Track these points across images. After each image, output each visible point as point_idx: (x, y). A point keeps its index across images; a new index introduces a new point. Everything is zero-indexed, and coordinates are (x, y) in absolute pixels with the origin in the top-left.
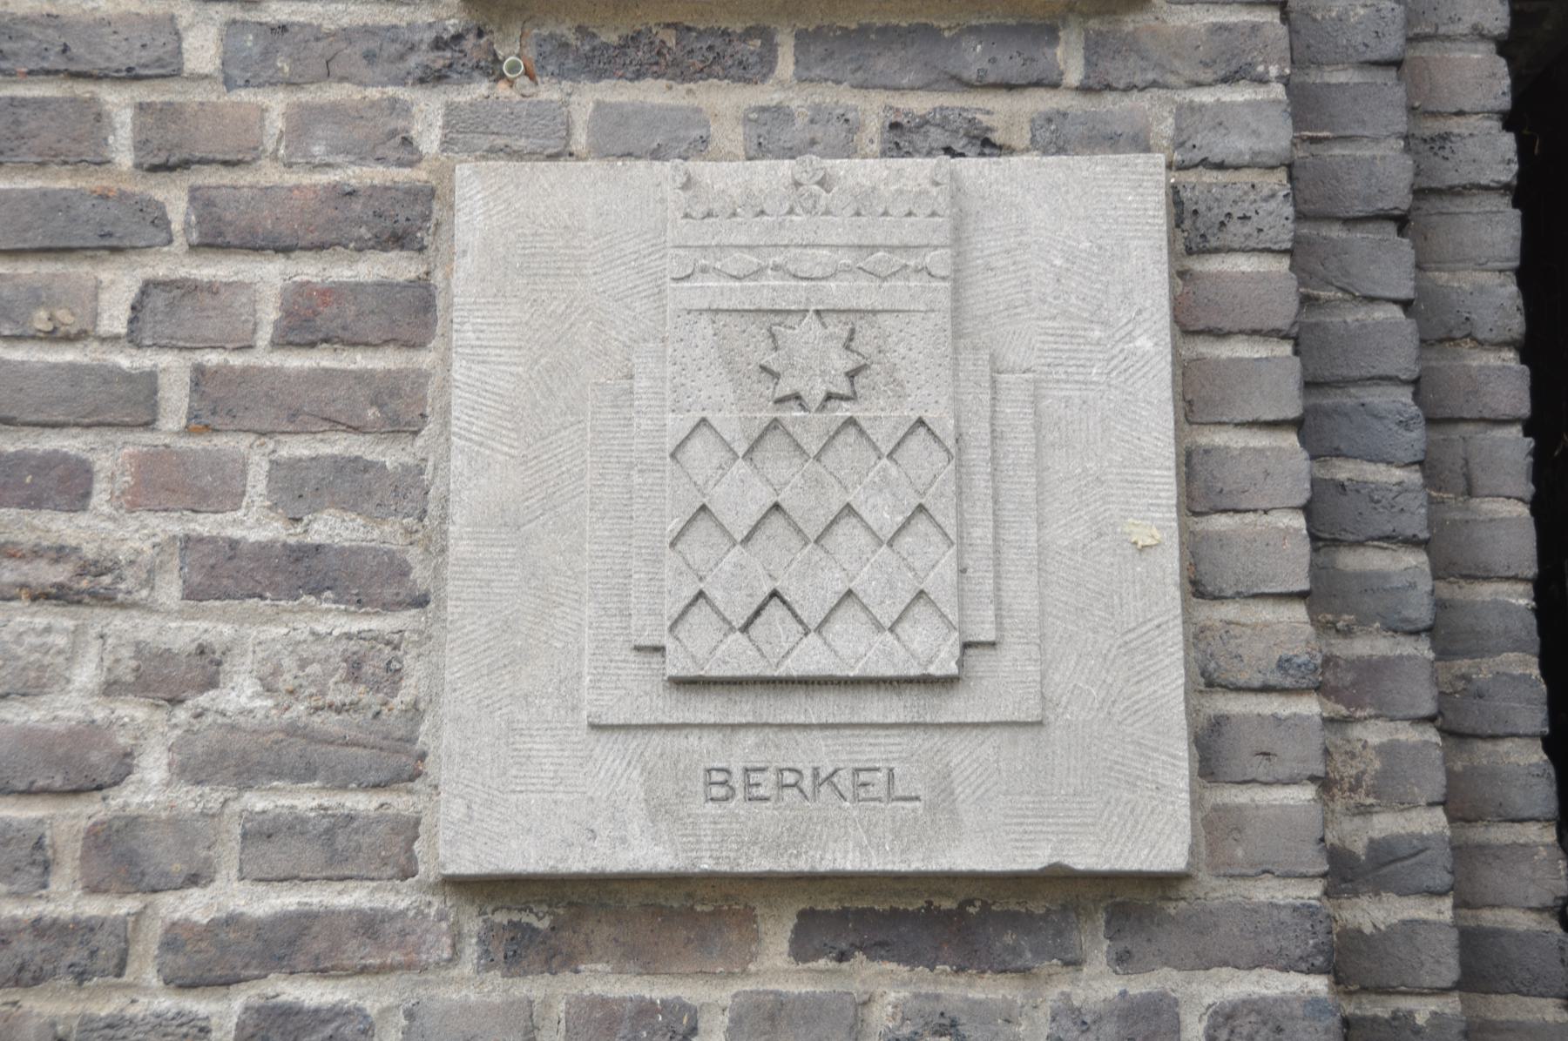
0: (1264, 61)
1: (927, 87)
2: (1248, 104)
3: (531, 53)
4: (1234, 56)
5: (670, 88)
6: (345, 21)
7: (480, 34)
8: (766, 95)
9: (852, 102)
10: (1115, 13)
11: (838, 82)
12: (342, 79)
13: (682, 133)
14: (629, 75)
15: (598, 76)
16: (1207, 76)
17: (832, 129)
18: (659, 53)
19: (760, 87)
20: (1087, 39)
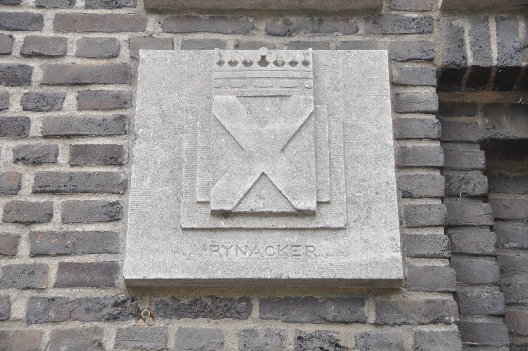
0: (448, 315)
1: (313, 322)
2: (443, 332)
3: (153, 308)
4: (436, 313)
5: (209, 321)
6: (79, 296)
7: (133, 300)
8: (247, 325)
9: (282, 328)
10: (387, 294)
11: (277, 320)
12: (76, 319)
13: (213, 340)
14: (192, 316)
15: (180, 317)
16: (426, 320)
17: (274, 339)
18: (205, 308)
19: (245, 321)
20: (376, 304)
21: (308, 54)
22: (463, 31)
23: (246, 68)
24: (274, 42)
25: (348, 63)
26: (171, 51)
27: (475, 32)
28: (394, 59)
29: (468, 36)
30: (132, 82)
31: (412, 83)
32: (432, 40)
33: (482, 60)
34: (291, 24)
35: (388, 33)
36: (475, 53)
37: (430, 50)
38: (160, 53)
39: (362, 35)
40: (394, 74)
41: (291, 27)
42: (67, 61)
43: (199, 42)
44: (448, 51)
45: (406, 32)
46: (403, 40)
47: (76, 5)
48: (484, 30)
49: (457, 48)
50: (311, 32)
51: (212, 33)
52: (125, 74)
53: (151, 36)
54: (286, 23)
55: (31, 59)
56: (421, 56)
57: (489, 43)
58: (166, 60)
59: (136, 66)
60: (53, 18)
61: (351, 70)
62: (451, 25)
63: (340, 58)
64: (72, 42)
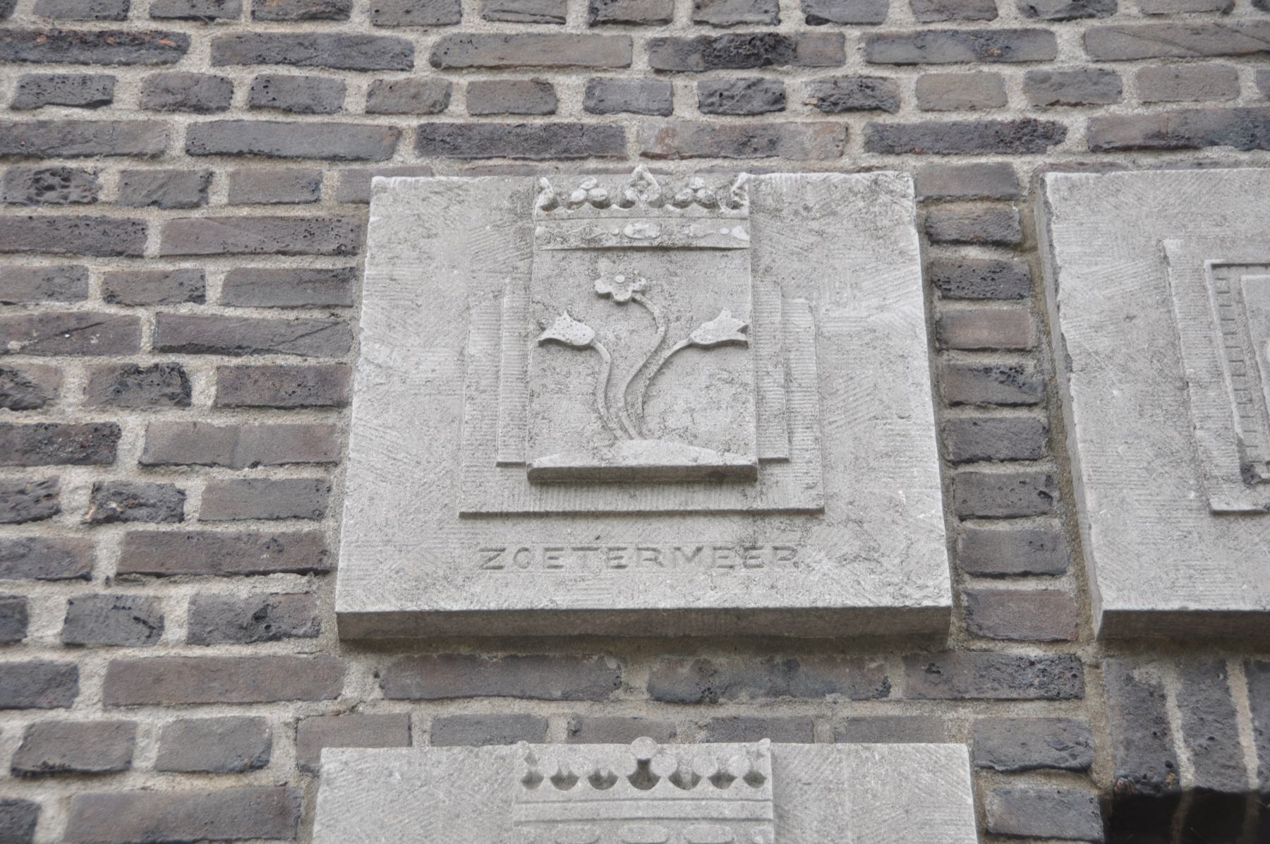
21: (759, 755)
22: (1163, 697)
23: (598, 793)
24: (673, 719)
25: (864, 776)
26: (404, 750)
27: (1194, 699)
28: (984, 767)
29: (1176, 710)
30: (300, 834)
31: (1036, 832)
32: (1082, 717)
33: (1218, 774)
34: (716, 672)
35: (967, 696)
36: (1200, 755)
37: (1078, 744)
38: (374, 755)
39: (899, 701)
40: (988, 808)
41: (716, 681)
42: (131, 783)
43: (478, 723)
44: (1127, 749)
45: (1015, 695)
46: (1006, 716)
47: (164, 637)
48: (1218, 695)
49: (1149, 740)
50: (767, 695)
51: (511, 699)
52: (283, 812)
53: (353, 709)
54: (703, 669)
55: (37, 784)
56: (1056, 761)
57: (1234, 727)
58: (391, 775)
59: (311, 792)
60: (103, 672)
61: (874, 796)
62: (1129, 679)
63: (844, 764)
64: (147, 734)
